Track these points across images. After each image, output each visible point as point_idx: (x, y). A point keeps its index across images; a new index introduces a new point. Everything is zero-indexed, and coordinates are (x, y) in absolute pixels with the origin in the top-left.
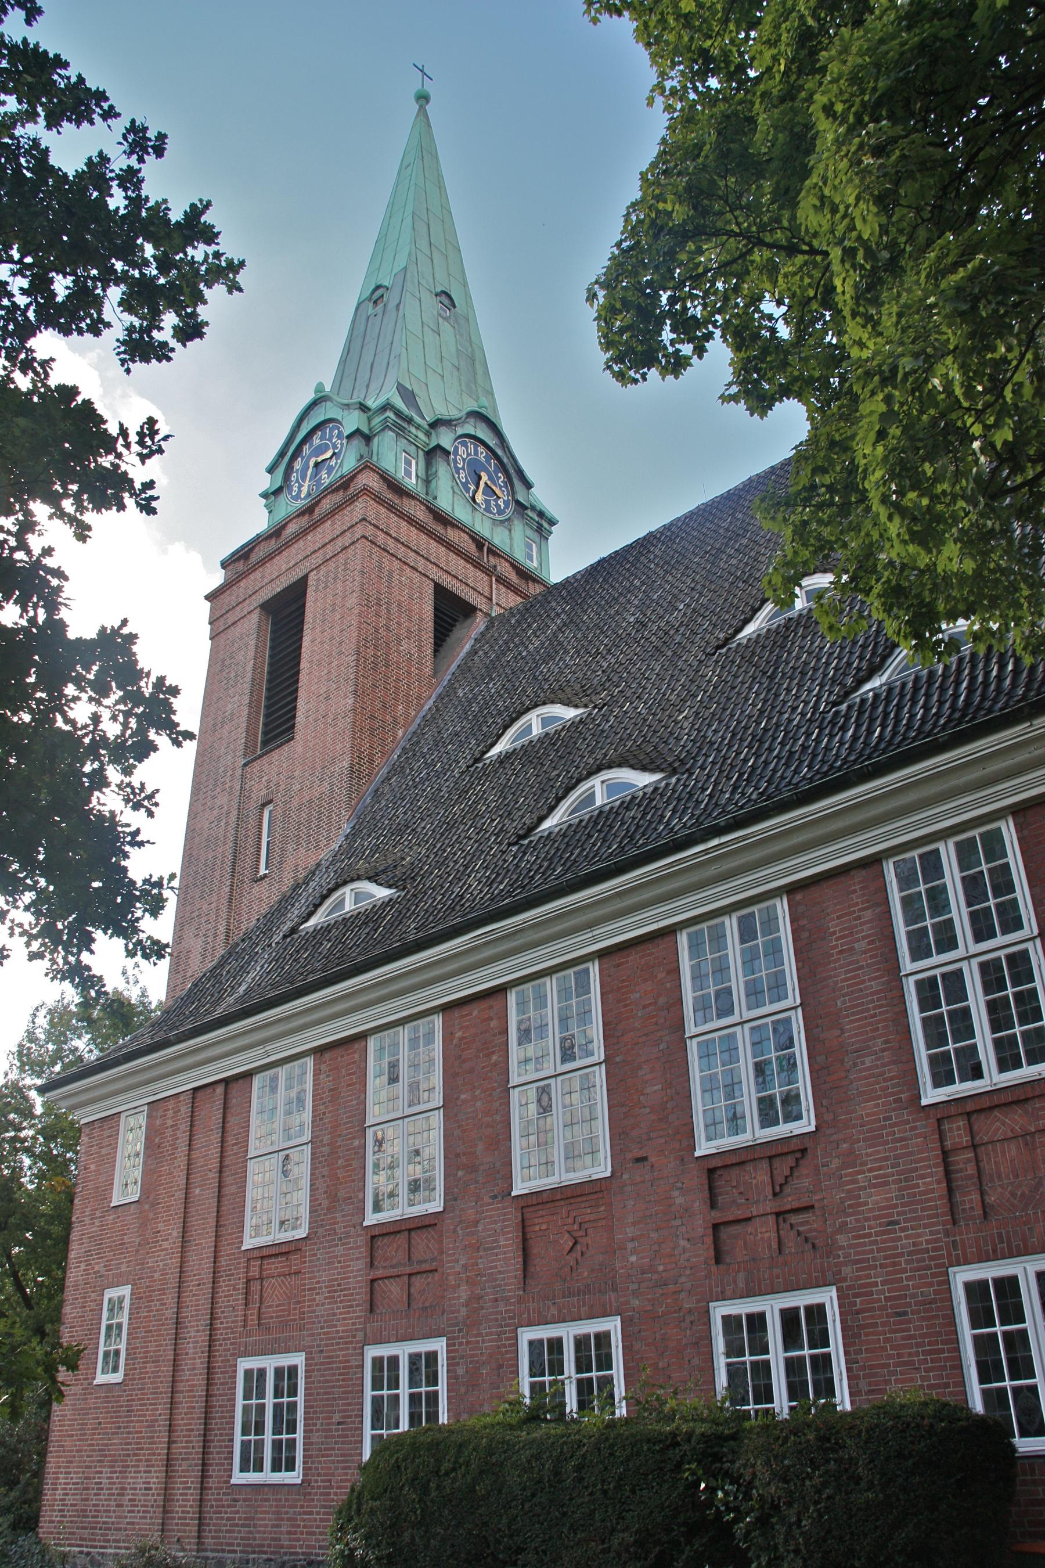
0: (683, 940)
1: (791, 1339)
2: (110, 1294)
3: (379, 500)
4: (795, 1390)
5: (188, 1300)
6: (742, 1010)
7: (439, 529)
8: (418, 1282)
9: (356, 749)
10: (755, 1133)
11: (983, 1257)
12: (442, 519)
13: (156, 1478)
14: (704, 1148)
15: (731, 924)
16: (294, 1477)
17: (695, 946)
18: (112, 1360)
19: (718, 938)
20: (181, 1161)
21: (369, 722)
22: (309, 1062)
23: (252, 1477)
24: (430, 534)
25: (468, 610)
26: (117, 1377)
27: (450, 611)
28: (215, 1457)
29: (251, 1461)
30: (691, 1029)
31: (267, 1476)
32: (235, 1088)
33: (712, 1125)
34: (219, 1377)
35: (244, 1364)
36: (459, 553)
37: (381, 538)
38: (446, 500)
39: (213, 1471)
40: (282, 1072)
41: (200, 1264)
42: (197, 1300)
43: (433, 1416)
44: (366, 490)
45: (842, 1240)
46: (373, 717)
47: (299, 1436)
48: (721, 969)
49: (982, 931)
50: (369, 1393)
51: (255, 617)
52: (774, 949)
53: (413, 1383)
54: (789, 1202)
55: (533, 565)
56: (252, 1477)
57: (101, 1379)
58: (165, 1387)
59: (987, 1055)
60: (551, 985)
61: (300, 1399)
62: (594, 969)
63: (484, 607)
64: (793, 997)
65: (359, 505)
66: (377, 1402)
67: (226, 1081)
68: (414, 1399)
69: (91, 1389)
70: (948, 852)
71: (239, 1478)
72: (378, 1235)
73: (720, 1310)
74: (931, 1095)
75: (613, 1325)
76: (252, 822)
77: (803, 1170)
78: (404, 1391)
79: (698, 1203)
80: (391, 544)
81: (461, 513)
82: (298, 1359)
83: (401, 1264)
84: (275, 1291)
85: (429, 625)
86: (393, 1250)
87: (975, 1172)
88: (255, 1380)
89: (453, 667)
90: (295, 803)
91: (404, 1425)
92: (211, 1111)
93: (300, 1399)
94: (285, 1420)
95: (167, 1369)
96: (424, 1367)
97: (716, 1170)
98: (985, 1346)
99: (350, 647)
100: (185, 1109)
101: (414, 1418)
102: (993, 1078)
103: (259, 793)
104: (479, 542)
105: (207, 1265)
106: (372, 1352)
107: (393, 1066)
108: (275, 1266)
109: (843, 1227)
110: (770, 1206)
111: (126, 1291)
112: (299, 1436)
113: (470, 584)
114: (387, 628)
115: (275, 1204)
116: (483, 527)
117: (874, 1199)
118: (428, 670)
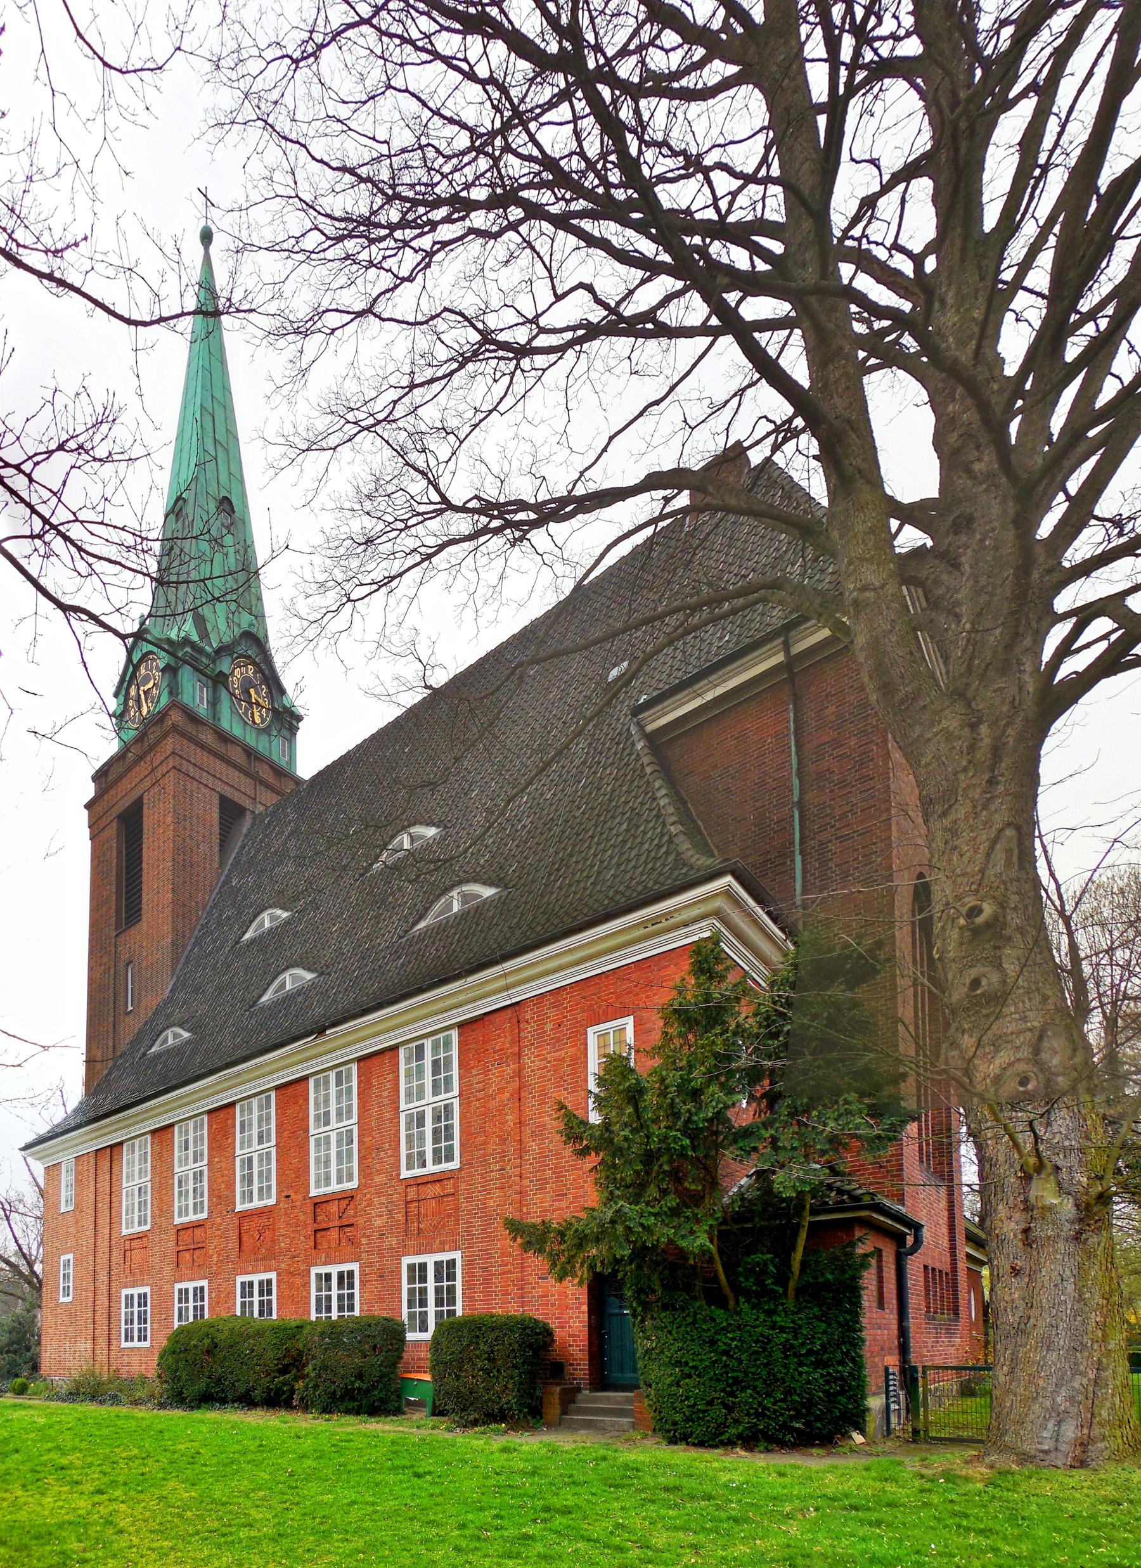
0: (311, 1082)
1: (422, 1154)
2: (64, 1258)
3: (183, 734)
4: (341, 1308)
5: (98, 1261)
6: (334, 1124)
7: (221, 749)
8: (197, 1252)
9: (175, 930)
10: (334, 1187)
11: (416, 1253)
12: (225, 738)
13: (89, 1345)
14: (314, 1192)
15: (332, 1075)
16: (147, 1344)
17: (317, 1086)
18: (66, 1290)
19: (327, 1082)
20: (92, 1189)
21: (181, 909)
22: (149, 1137)
23: (129, 1344)
24: (216, 755)
25: (240, 811)
26: (70, 1299)
27: (230, 812)
28: (113, 1336)
29: (129, 1337)
30: (312, 1131)
31: (136, 1344)
32: (115, 1150)
33: (318, 1181)
34: (114, 1298)
35: (125, 1292)
36: (235, 766)
37: (185, 766)
38: (228, 722)
39: (113, 1342)
40: (137, 1142)
41: (103, 1245)
42: (102, 1259)
43: (202, 1316)
44: (175, 728)
45: (364, 1241)
46: (184, 905)
47: (148, 1325)
48: (327, 1101)
49: (436, 1091)
50: (177, 1305)
51: (114, 824)
52: (349, 1090)
53: (195, 1301)
54: (345, 1222)
55: (283, 762)
56: (129, 1344)
57: (62, 1300)
58: (90, 1303)
59: (429, 1157)
60: (255, 1102)
61: (148, 1308)
62: (273, 1094)
63: (251, 807)
64: (355, 1119)
65: (170, 740)
66: (180, 1309)
67: (111, 1146)
68: (195, 1308)
69: (58, 1305)
70: (428, 1044)
71: (124, 1345)
72: (181, 1229)
73: (314, 1271)
74: (405, 1174)
75: (273, 1276)
76: (122, 972)
77: (352, 1206)
78: (191, 1304)
79: (310, 1221)
80: (192, 770)
81: (237, 731)
82: (147, 1289)
83: (190, 1245)
84: (137, 1256)
85: (216, 828)
86: (185, 1236)
87: (981, 318)
88: (130, 1299)
89: (231, 860)
90: (144, 964)
91: (191, 1319)
92: (105, 1165)
93: (148, 1308)
94: (143, 1319)
95: (91, 1295)
96: (199, 1293)
97: (318, 1204)
98: (411, 1292)
99: (168, 855)
100: (92, 1161)
101: (195, 1316)
102: (431, 1168)
103: (124, 957)
104: (250, 753)
105: (106, 1243)
106: (178, 1286)
107: (186, 1141)
108: (136, 1244)
109: (364, 1236)
110: (337, 1223)
111: (70, 1256)
112: (148, 1325)
113: (240, 789)
114: (190, 836)
115: (133, 1221)
116: (251, 739)
117: (377, 1222)
118: (216, 865)
